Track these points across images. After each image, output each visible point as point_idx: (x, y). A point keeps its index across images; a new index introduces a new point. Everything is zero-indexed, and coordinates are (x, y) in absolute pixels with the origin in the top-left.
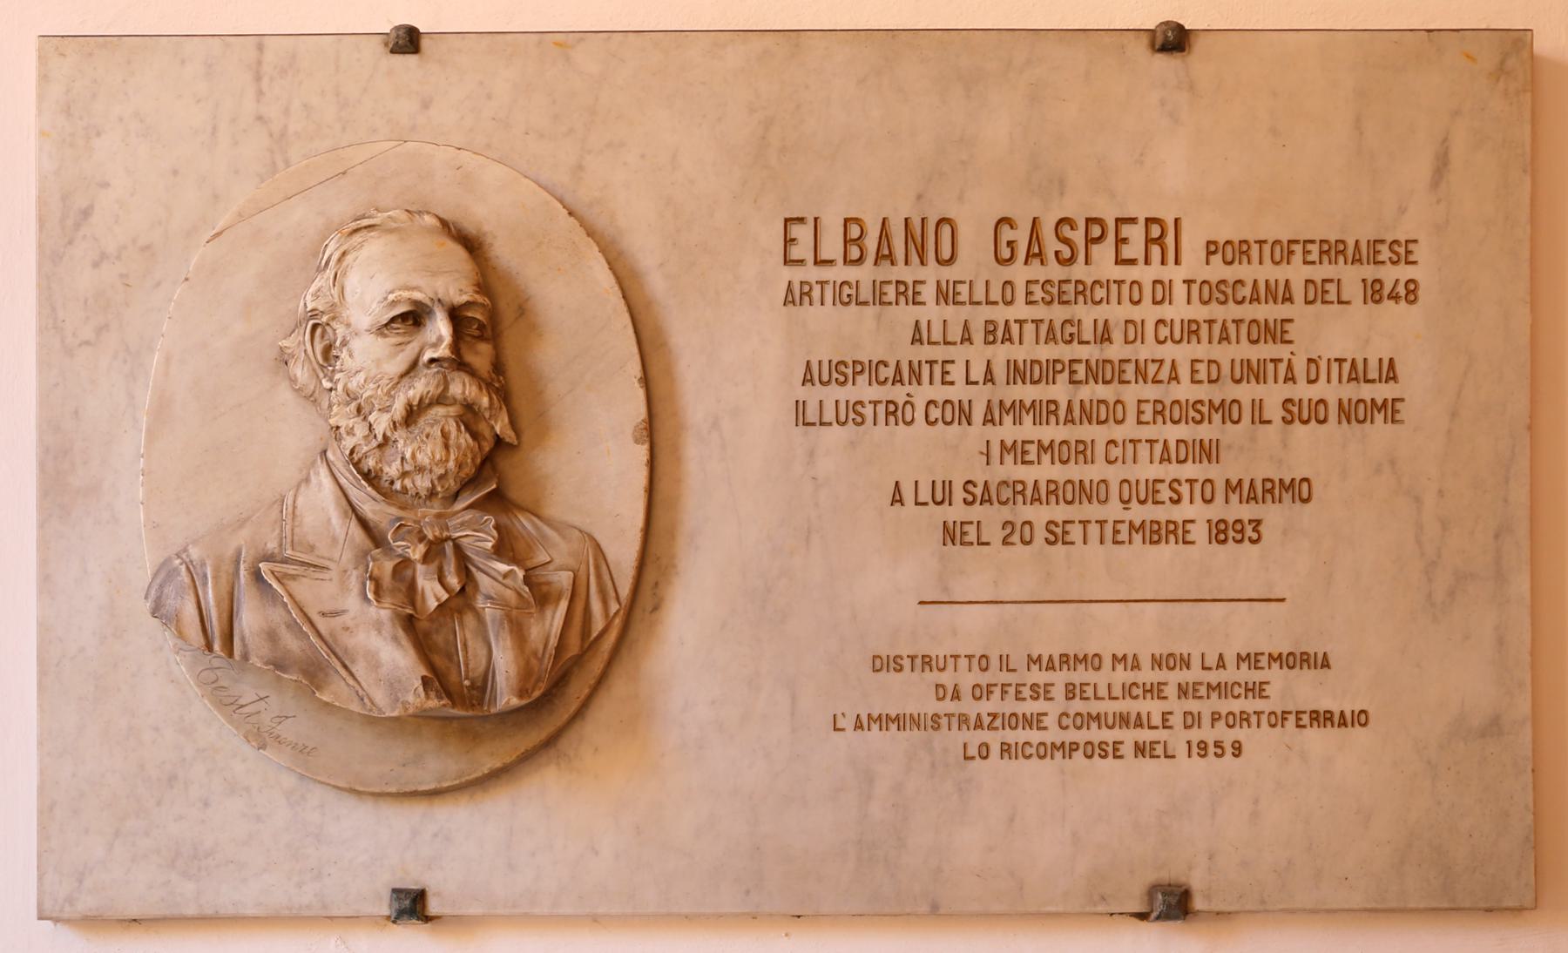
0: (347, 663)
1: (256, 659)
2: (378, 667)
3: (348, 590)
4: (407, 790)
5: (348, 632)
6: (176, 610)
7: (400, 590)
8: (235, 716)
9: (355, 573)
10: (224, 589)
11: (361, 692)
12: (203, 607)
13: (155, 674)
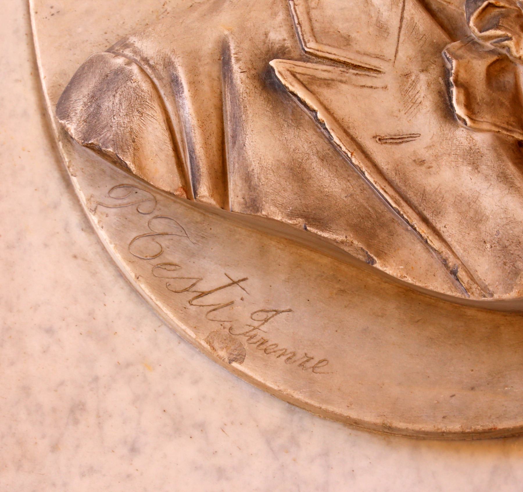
0: (428, 215)
1: (273, 208)
2: (479, 221)
3: (416, 104)
4: (479, 428)
5: (423, 168)
6: (131, 132)
7: (502, 104)
8: (192, 309)
9: (423, 77)
10: (210, 103)
11: (452, 261)
12: (176, 128)
13: (46, 245)
